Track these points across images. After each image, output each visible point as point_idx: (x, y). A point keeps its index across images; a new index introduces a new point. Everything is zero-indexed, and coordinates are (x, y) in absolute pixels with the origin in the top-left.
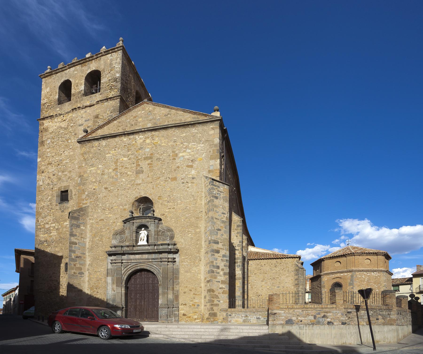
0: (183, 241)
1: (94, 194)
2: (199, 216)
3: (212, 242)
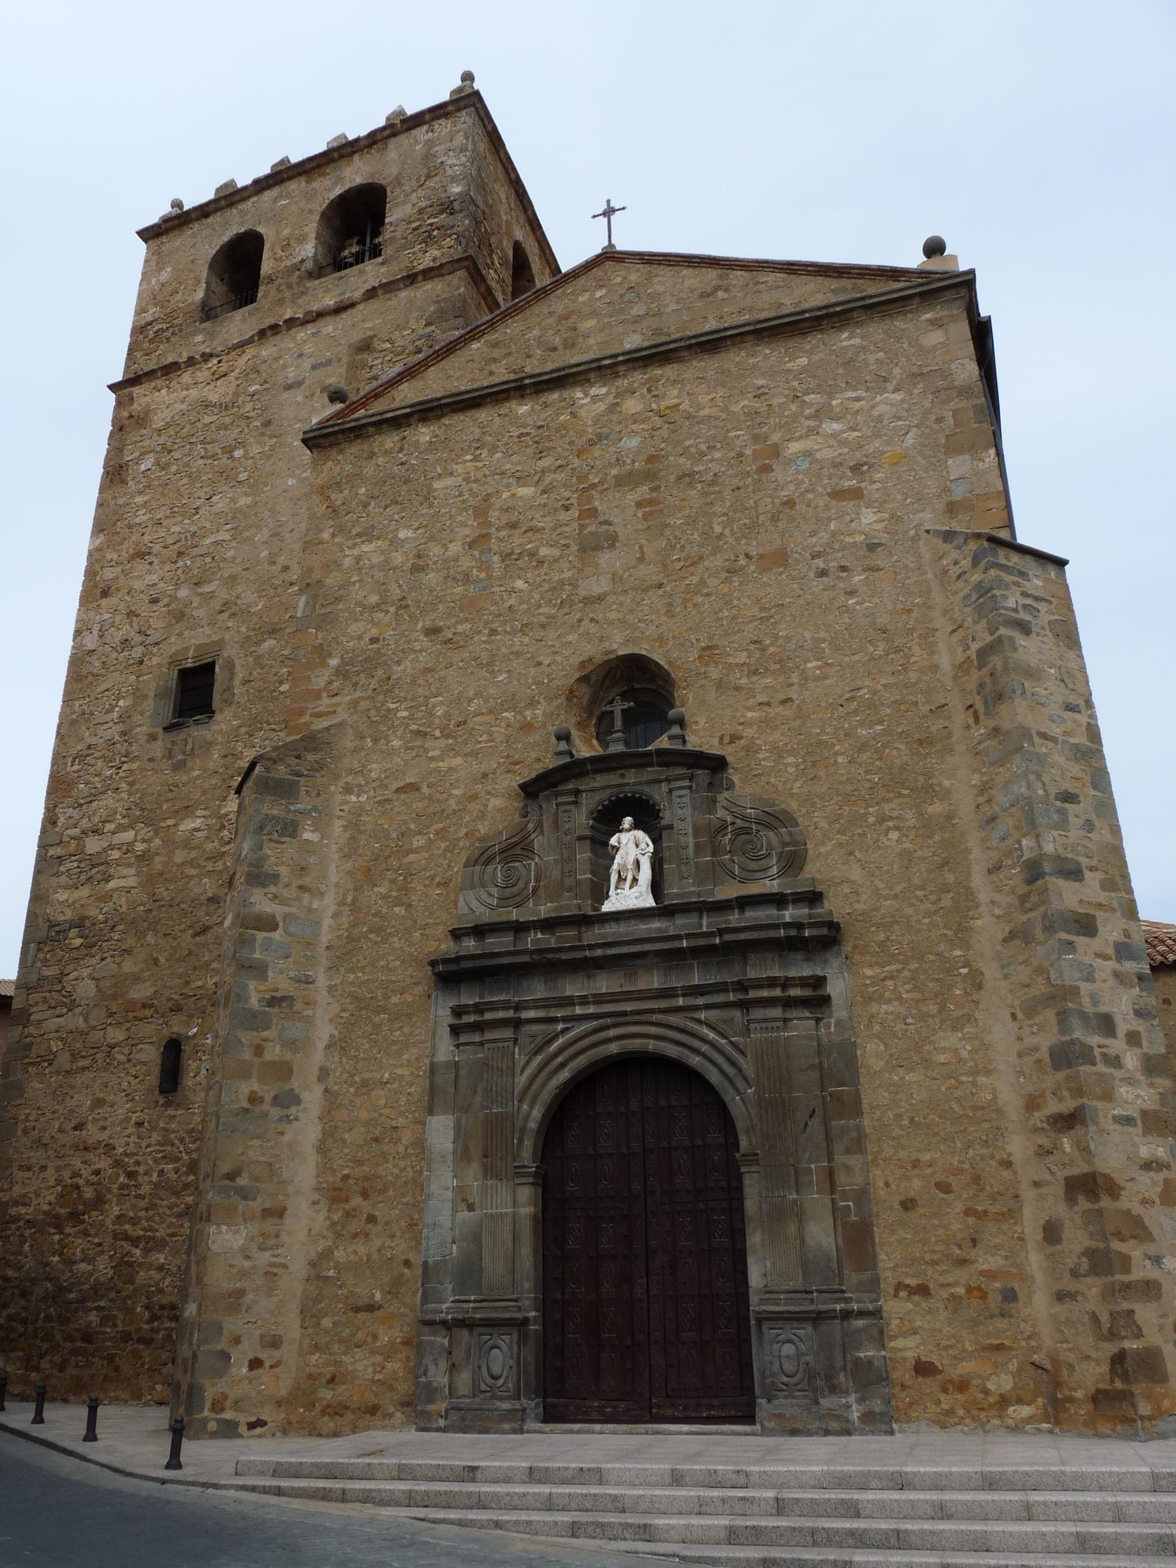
0: (856, 874)
1: (371, 663)
2: (934, 729)
3: (1047, 867)
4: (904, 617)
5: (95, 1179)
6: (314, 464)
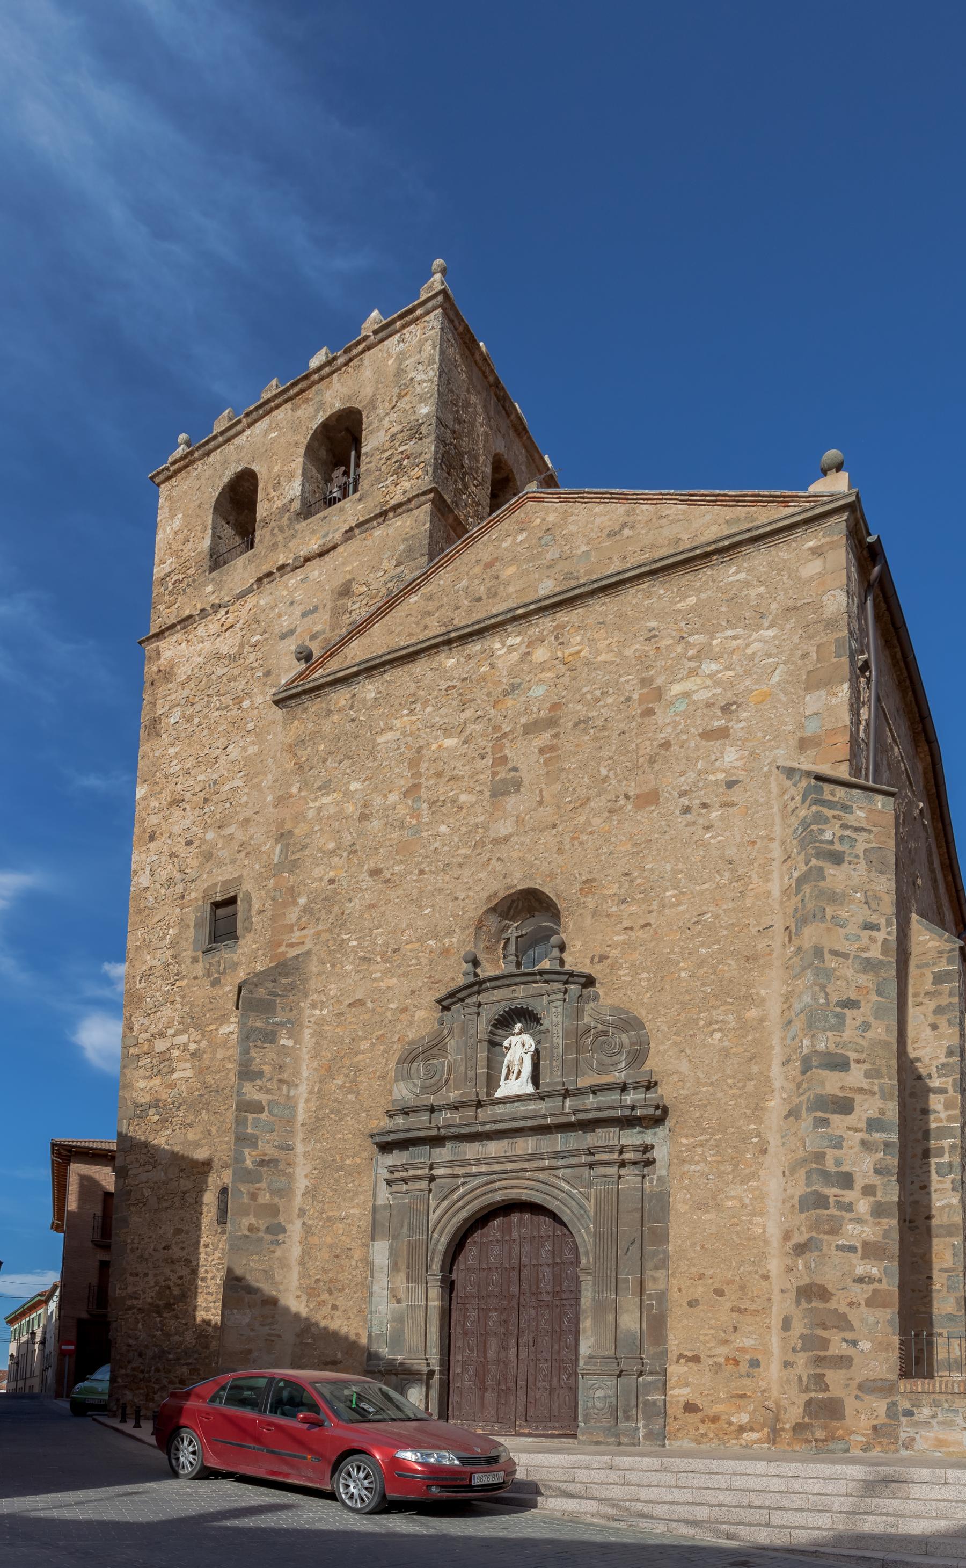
0: (684, 1067)
1: (329, 900)
4: (749, 848)
5: (180, 1282)
6: (286, 722)
